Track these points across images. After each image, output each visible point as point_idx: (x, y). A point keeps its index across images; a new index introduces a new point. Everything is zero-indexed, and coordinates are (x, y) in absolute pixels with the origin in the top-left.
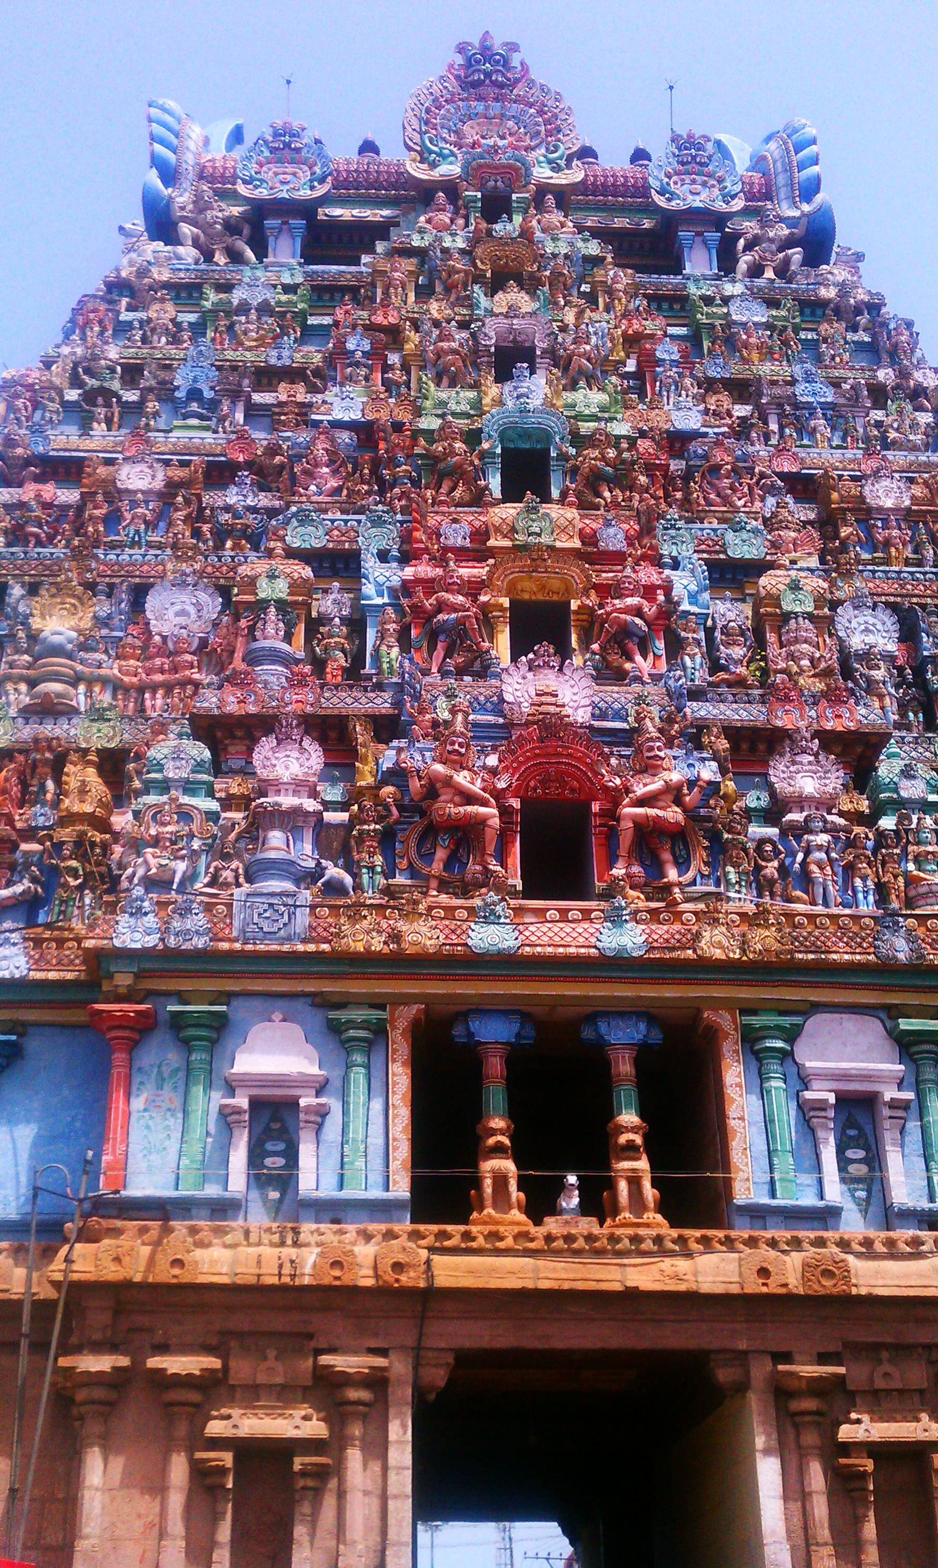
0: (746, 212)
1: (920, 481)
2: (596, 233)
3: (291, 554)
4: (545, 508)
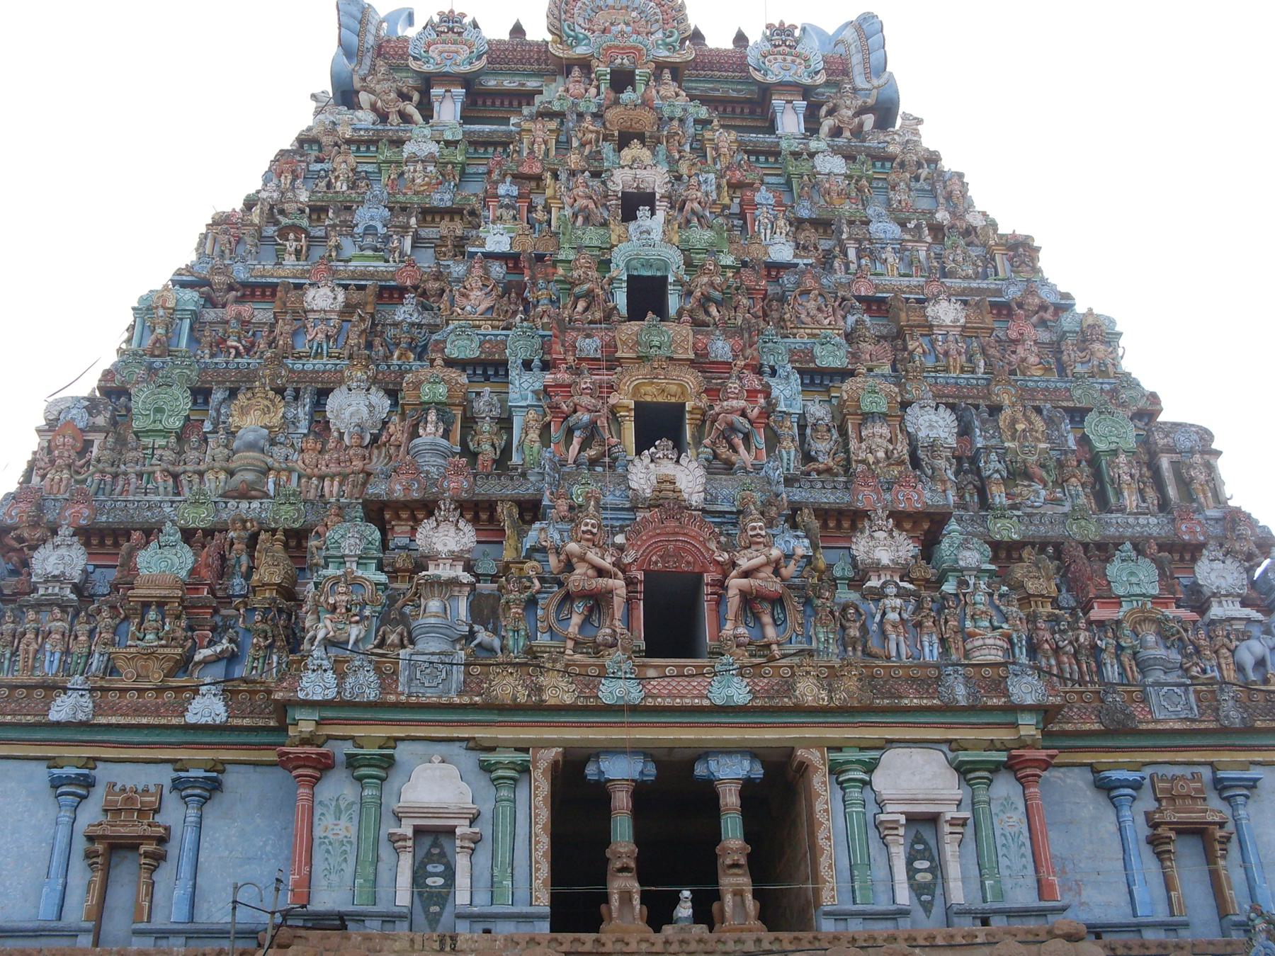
0: (827, 84)
1: (972, 303)
2: (705, 101)
3: (450, 363)
4: (664, 326)
